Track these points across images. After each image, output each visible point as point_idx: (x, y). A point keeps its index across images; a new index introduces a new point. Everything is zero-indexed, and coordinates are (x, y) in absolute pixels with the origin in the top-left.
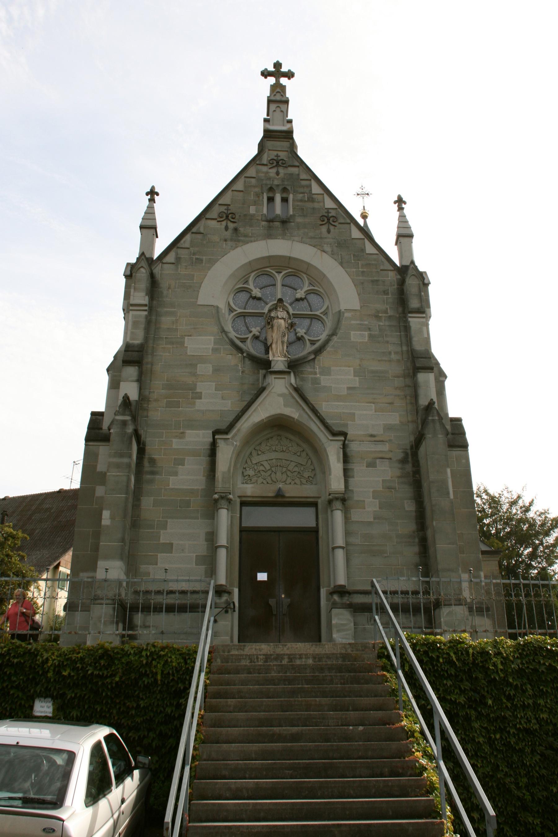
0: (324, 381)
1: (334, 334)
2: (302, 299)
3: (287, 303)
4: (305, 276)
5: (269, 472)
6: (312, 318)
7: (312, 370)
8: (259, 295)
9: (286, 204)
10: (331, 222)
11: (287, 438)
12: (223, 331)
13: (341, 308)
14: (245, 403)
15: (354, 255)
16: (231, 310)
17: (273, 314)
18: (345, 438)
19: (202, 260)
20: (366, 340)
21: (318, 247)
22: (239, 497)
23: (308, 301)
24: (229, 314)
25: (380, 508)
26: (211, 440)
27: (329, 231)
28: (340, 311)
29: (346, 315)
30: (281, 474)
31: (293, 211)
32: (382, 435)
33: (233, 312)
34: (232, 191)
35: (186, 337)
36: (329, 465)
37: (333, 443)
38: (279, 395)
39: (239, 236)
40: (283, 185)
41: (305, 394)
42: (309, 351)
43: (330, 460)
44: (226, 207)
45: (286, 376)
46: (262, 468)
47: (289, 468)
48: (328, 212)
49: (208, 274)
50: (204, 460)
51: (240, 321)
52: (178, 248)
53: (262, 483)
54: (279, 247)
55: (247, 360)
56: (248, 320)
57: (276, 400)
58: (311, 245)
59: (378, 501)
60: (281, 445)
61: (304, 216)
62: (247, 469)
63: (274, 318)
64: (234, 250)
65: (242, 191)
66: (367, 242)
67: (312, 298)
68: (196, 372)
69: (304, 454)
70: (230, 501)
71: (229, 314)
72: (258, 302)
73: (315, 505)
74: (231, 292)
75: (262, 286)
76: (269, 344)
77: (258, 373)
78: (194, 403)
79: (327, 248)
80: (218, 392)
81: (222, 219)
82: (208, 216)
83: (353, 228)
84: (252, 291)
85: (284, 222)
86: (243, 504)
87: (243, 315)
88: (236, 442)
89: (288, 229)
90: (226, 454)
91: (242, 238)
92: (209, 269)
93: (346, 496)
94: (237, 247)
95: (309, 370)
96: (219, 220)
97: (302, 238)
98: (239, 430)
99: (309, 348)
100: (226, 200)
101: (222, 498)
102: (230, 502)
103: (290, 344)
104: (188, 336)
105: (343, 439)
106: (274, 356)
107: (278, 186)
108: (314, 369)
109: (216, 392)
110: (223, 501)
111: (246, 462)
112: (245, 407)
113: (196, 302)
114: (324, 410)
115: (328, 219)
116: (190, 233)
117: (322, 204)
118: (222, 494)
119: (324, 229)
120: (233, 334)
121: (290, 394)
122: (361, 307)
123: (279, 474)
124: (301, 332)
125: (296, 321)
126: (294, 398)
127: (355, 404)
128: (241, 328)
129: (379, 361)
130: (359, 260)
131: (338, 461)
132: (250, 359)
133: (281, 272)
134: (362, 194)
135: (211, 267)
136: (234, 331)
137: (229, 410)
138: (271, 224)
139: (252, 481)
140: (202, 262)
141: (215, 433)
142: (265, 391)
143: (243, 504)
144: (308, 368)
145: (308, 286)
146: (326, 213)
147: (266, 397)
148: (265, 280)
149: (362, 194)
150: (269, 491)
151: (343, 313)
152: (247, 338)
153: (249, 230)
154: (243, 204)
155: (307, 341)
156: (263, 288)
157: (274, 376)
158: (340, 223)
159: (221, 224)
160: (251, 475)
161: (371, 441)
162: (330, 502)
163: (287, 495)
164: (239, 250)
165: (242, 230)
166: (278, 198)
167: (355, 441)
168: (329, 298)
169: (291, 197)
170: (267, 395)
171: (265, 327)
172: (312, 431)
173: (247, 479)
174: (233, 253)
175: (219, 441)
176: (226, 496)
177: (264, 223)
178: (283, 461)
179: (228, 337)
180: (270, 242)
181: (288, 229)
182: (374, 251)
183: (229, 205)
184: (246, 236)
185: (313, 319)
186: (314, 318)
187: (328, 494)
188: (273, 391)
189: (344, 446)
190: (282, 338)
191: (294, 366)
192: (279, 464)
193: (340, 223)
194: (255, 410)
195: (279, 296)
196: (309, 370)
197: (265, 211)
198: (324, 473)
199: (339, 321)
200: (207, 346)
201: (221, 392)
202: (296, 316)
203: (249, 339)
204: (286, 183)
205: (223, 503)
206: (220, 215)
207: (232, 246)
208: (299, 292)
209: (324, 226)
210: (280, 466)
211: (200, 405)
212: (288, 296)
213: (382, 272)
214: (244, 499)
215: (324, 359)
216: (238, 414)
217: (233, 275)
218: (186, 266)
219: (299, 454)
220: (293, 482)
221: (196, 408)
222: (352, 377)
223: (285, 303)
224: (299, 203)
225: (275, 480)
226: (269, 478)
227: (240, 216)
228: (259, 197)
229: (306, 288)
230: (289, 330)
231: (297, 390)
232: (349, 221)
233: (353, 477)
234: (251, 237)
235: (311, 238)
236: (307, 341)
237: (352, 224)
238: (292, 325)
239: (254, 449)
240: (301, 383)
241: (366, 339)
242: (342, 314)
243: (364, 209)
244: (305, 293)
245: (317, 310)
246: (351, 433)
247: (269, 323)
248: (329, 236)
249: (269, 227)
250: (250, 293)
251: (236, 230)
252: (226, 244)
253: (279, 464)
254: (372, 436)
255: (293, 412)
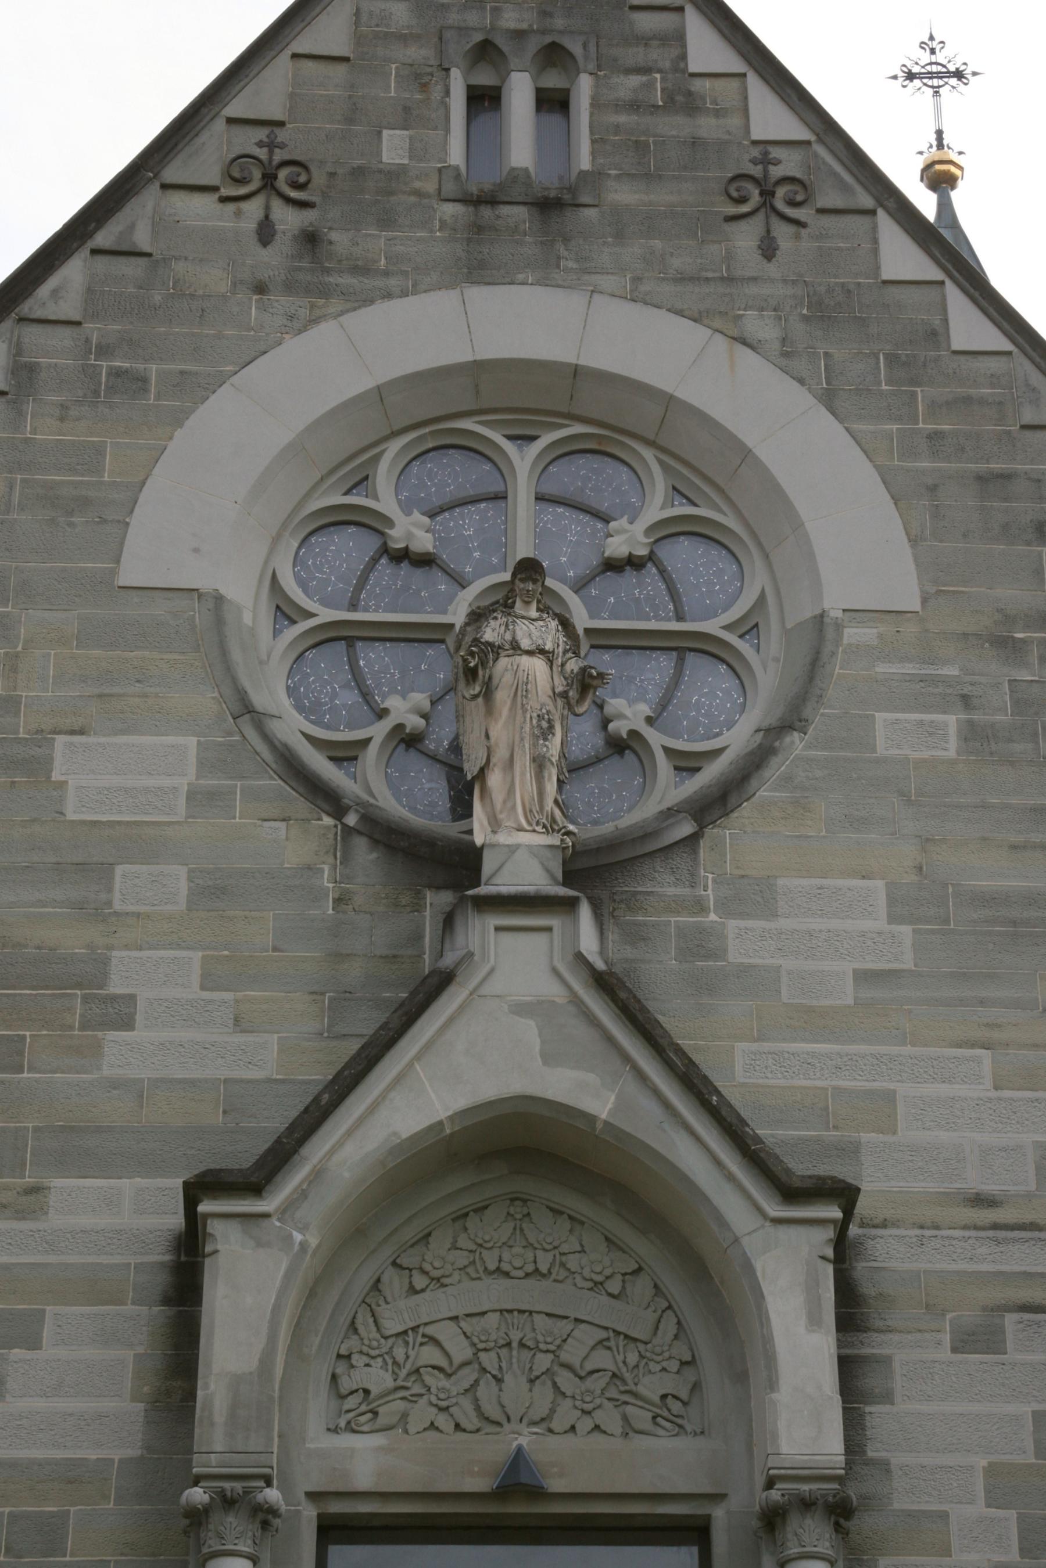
0: (744, 941)
1: (790, 721)
2: (634, 563)
3: (563, 580)
4: (648, 454)
5: (468, 1376)
6: (681, 651)
7: (687, 891)
8: (424, 542)
9: (555, 120)
10: (780, 205)
11: (557, 1212)
12: (245, 709)
13: (826, 605)
14: (353, 1046)
15: (892, 360)
16: (286, 612)
17: (491, 632)
18: (848, 1212)
19: (142, 381)
20: (952, 753)
21: (717, 323)
22: (313, 1496)
23: (662, 572)
24: (276, 633)
25: (1023, 1552)
26: (177, 1221)
27: (768, 249)
28: (820, 618)
29: (852, 634)
30: (526, 1386)
31: (594, 154)
32: (1029, 1196)
33: (293, 622)
34: (295, 56)
35: (61, 740)
36: (768, 1341)
37: (785, 1233)
38: (521, 1009)
39: (328, 271)
40: (543, 32)
41: (650, 1005)
42: (664, 806)
43: (772, 1316)
44: (262, 133)
45: (554, 922)
46: (430, 1355)
47: (564, 1357)
48: (765, 161)
49: (172, 446)
50: (140, 1321)
51: (328, 667)
52: (21, 320)
53: (432, 1426)
54: (525, 321)
55: (361, 844)
56: (373, 658)
57: (509, 1031)
58: (680, 313)
59: (1012, 1514)
60: (529, 1245)
61: (649, 178)
62: (357, 1360)
63: (496, 650)
64: (300, 332)
65: (346, 59)
66: (956, 299)
67: (681, 555)
68: (109, 903)
69: (641, 1288)
70: (265, 1517)
71: (276, 633)
72: (419, 574)
73: (695, 1532)
74: (284, 525)
75: (436, 502)
76: (471, 769)
77: (418, 907)
78: (96, 1049)
79: (760, 326)
80: (216, 995)
81: (243, 191)
82: (172, 173)
83: (888, 229)
84: (389, 522)
85: (551, 206)
86: (334, 1530)
87: (343, 637)
88: (302, 1230)
89: (566, 240)
90: (249, 1288)
91: (346, 280)
92: (179, 423)
93: (853, 1493)
94: (315, 321)
95: (671, 891)
96: (225, 192)
97: (637, 280)
98: (318, 1175)
99: (670, 789)
100: (267, 95)
101: (228, 1502)
102: (265, 1525)
103: (574, 769)
104: (72, 732)
105: (837, 1214)
106: (495, 824)
107: (519, 35)
108: (693, 885)
109: (206, 995)
110: (231, 1519)
111: (353, 1327)
112: (347, 1066)
113: (114, 573)
114: (740, 1076)
115: (767, 194)
116: (84, 253)
117: (734, 122)
118: (227, 1485)
119: (745, 238)
120: (292, 726)
121: (576, 1001)
122: (924, 601)
123: (515, 1384)
124: (630, 713)
125: (604, 661)
126: (593, 1021)
127: (895, 1050)
128: (334, 695)
129: (1014, 847)
130: (915, 382)
131: (814, 1321)
132: (375, 842)
133: (533, 438)
134: (931, 75)
135: (188, 413)
136: (300, 708)
137: (270, 1081)
138: (486, 212)
139: (381, 1421)
140: (145, 390)
141: (196, 1190)
142: (452, 989)
143: (334, 1530)
144: (663, 884)
145: (668, 503)
146: (754, 162)
147: (451, 1020)
148: (453, 475)
149: (931, 75)
150: (465, 1467)
151: (839, 626)
152: (366, 742)
153: (376, 243)
154: (350, 120)
155: (660, 756)
156: (442, 510)
157: (494, 920)
158: (822, 211)
159: (238, 214)
160: (375, 1391)
161: (976, 1228)
162: (772, 1520)
163: (556, 1485)
164: (326, 332)
165: (340, 239)
166: (520, 92)
167: (896, 1224)
168: (766, 556)
169: (584, 89)
170: (462, 1008)
171: (451, 689)
172: (684, 1178)
173: (357, 1409)
174: (294, 349)
175: (215, 1227)
176: (247, 1492)
177: (450, 210)
178: (539, 1320)
179: (267, 738)
180: (476, 294)
181: (566, 240)
182: (994, 339)
183: (281, 124)
184: (362, 269)
185: (691, 658)
186: (687, 647)
187: (760, 1481)
188: (485, 990)
189: (843, 1253)
190: (535, 745)
191: (593, 872)
192: (515, 1336)
193: (822, 211)
194: (398, 1080)
195: (524, 550)
196: (671, 891)
197: (456, 155)
198: (741, 1377)
199: (815, 666)
200: (167, 782)
201: (228, 996)
202: (604, 640)
203: (373, 749)
204: (559, 23)
205: (233, 1526)
206: (235, 172)
207: (291, 318)
208: (620, 531)
209: (743, 225)
210: (522, 1345)
211: (123, 1054)
212: (567, 548)
213: (1028, 434)
214: (336, 1507)
215: (742, 842)
216: (316, 1099)
217: (295, 450)
218: (63, 407)
219: (614, 1286)
220: (587, 1424)
221: (106, 1072)
222: (879, 923)
223: (549, 582)
224: (622, 119)
225: (496, 1414)
226: (466, 1403)
227: (332, 175)
228: (424, 87)
229: (654, 511)
230: (569, 706)
231: (605, 983)
232: (866, 201)
233: (887, 1398)
234: (386, 274)
235: (682, 279)
236: (660, 756)
237: (880, 212)
238: (586, 683)
239: (394, 1264)
240: (629, 952)
241: (951, 749)
242: (830, 633)
243: (940, 145)
244: (650, 530)
245: (710, 614)
246: (875, 1186)
247: (471, 674)
248: (772, 269)
249: (478, 229)
250: (382, 534)
251: (311, 239)
252: (262, 308)
253: (515, 1336)
254: (980, 1201)
255: (591, 1089)
